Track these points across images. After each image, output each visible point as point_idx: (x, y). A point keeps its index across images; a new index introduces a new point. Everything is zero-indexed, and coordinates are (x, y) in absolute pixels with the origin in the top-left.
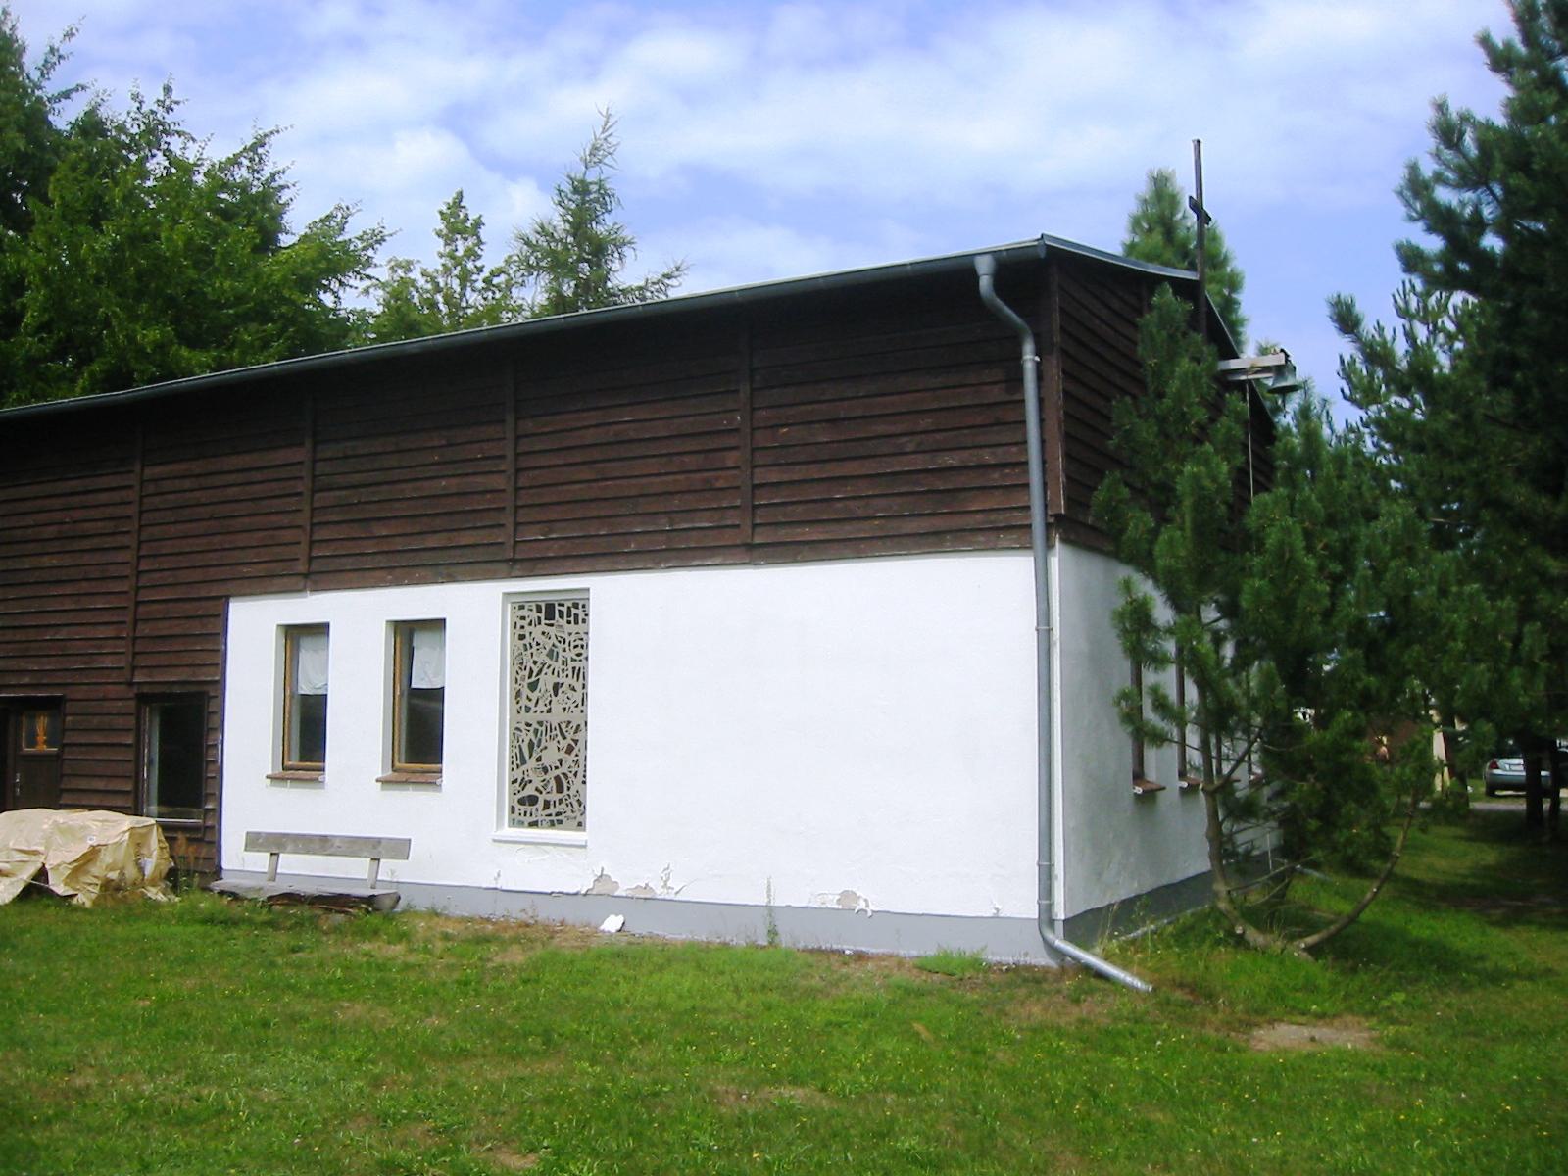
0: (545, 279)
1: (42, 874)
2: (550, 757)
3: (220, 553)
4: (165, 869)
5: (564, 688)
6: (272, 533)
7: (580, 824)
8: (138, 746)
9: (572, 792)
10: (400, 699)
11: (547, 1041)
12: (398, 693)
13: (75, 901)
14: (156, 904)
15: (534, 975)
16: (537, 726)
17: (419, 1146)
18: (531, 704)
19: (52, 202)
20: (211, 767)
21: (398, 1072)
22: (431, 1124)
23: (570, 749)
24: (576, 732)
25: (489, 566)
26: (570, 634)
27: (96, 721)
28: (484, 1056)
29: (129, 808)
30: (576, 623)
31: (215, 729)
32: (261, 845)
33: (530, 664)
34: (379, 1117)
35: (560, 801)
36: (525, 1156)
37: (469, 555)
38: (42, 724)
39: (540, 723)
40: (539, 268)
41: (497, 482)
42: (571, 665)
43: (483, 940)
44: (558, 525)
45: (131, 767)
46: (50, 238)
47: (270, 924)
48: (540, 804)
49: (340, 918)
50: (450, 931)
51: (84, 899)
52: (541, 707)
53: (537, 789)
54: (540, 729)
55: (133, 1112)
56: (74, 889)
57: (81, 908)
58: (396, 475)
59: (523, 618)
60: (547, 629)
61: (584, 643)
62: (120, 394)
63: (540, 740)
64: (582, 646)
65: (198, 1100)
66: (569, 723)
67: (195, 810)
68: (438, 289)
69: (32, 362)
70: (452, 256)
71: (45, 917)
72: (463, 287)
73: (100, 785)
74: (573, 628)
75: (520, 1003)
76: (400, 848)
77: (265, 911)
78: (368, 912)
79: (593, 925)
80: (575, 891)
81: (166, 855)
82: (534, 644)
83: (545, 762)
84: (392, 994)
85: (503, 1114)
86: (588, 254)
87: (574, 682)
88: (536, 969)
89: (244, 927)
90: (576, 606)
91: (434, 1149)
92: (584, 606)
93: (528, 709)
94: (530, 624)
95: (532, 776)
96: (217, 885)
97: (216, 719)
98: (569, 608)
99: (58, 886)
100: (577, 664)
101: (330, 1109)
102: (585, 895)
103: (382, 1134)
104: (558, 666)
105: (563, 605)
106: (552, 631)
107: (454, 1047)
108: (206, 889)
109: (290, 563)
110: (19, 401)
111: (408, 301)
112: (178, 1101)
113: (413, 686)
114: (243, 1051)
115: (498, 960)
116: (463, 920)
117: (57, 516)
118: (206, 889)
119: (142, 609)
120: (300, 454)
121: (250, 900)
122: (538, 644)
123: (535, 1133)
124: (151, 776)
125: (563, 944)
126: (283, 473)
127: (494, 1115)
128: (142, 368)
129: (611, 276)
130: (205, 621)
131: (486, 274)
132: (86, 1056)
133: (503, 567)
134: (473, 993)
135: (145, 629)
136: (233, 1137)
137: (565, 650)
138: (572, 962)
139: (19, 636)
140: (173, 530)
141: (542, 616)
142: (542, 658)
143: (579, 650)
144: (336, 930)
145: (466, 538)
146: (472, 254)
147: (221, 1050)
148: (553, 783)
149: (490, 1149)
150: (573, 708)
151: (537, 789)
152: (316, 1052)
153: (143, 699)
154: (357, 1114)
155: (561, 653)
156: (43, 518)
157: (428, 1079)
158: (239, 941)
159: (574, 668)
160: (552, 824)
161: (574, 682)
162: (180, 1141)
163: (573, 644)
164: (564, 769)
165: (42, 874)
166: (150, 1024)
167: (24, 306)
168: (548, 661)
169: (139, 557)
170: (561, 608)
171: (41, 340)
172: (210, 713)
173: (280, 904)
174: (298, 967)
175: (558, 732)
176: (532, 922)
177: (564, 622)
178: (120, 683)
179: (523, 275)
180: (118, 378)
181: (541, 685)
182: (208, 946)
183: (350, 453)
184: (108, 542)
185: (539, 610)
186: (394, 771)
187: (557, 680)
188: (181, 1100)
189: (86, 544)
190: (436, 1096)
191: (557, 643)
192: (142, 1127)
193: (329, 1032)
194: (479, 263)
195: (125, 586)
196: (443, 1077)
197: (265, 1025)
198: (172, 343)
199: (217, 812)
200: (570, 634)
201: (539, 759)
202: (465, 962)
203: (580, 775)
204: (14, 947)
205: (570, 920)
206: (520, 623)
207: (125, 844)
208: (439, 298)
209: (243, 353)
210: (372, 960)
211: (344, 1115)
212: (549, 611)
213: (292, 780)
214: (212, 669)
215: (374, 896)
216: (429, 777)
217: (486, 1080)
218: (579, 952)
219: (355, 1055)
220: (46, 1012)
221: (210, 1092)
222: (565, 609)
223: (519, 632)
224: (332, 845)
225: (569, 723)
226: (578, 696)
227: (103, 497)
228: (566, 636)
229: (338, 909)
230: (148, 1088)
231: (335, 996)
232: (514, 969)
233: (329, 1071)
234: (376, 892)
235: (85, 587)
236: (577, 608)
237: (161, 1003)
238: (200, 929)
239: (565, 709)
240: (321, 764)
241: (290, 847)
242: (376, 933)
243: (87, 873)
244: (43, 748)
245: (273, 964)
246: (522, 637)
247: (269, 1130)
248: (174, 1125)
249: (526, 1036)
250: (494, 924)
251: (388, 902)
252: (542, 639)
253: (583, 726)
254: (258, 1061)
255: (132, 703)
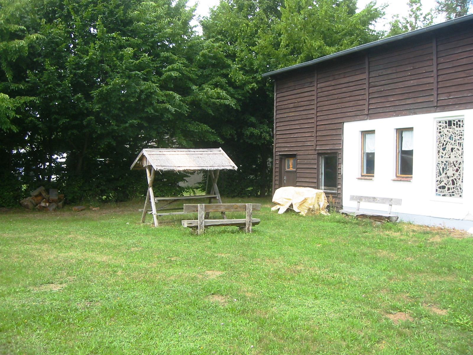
0: (445, 14)
1: (291, 205)
2: (450, 173)
3: (340, 109)
4: (327, 204)
5: (455, 149)
6: (356, 102)
7: (461, 196)
8: (318, 169)
9: (458, 185)
10: (398, 154)
11: (449, 270)
12: (398, 152)
13: (300, 214)
14: (324, 216)
15: (444, 246)
16: (446, 163)
17: (404, 302)
18: (443, 155)
19: (286, 7)
20: (339, 175)
21: (397, 275)
22: (408, 295)
23: (457, 170)
24: (459, 164)
25: (428, 109)
26: (457, 131)
27: (306, 161)
28: (427, 272)
29: (316, 187)
30: (460, 127)
31: (340, 163)
32: (354, 199)
33: (443, 142)
34: (391, 290)
35: (454, 188)
36: (442, 310)
37: (421, 106)
38: (291, 161)
39: (447, 162)
40: (442, 10)
41: (431, 80)
42: (458, 141)
43: (426, 233)
44: (453, 93)
45: (316, 175)
46: (287, 18)
47: (357, 224)
48: (446, 189)
49: (379, 223)
50: (415, 229)
51: (303, 213)
52: (447, 156)
53: (445, 184)
54: (446, 163)
55: (313, 279)
56: (300, 210)
57: (302, 216)
58: (396, 80)
59: (440, 126)
60: (449, 130)
61: (463, 134)
62: (310, 62)
63: (446, 167)
64: (462, 135)
65: (333, 278)
66: (457, 161)
67: (335, 188)
68: (407, 22)
69: (285, 56)
70: (412, 11)
71: (291, 218)
72: (416, 20)
73: (307, 180)
74: (458, 129)
75: (439, 255)
76: (399, 202)
77: (355, 219)
78: (388, 222)
79: (465, 230)
80: (458, 219)
81: (327, 201)
82: (444, 135)
83: (448, 175)
84: (396, 249)
85: (434, 294)
86: (460, 3)
87: (459, 147)
88: (445, 244)
89: (349, 224)
90: (459, 121)
91: (410, 304)
92: (462, 121)
93: (442, 157)
94: (443, 128)
95: (443, 179)
96: (341, 211)
97: (341, 160)
98: (457, 122)
99: (295, 209)
100: (460, 141)
101: (374, 285)
102: (462, 220)
103: (392, 295)
104: (453, 142)
105: (455, 121)
106: (451, 130)
107: (417, 268)
108: (338, 212)
109: (362, 111)
110: (281, 67)
111: (397, 27)
112: (327, 278)
113: (403, 149)
114: (348, 264)
115: (431, 240)
116: (419, 226)
117: (293, 101)
118: (338, 212)
119: (318, 127)
120: (365, 76)
121: (351, 216)
122: (446, 135)
123: (446, 302)
124: (322, 178)
125: (454, 236)
126: (360, 82)
127: (431, 294)
128: (315, 54)
129: (469, 10)
130: (337, 130)
131: (424, 15)
132: (301, 260)
133: (433, 109)
134: (423, 250)
135: (319, 134)
136: (344, 291)
137: (455, 136)
138: (458, 243)
139: (284, 136)
140: (326, 103)
141: (447, 125)
142: (447, 139)
143: (461, 136)
144: (377, 227)
145: (420, 100)
146: (418, 9)
147: (341, 262)
148: (451, 182)
149: (429, 306)
150: (458, 156)
151: (445, 184)
152: (371, 266)
153: (319, 154)
154: (384, 288)
155: (454, 138)
156: (289, 102)
157: (408, 279)
158: (348, 228)
159: (459, 143)
160: (451, 195)
161: (459, 147)
162: (327, 290)
163: (458, 134)
164: (455, 177)
165: (291, 205)
166: (320, 252)
167: (281, 40)
168: (449, 140)
169: (317, 112)
170: (454, 122)
171: (287, 49)
172: (339, 159)
173: (360, 218)
174: (366, 238)
175: (453, 165)
176: (443, 228)
177: (455, 127)
178: (313, 150)
179: (437, 14)
180: (309, 58)
181: (447, 148)
182: (338, 229)
183: (380, 74)
184: (308, 108)
185: (446, 123)
186: (396, 177)
187: (452, 147)
188: (328, 277)
189: (302, 109)
190: (410, 285)
191: (452, 134)
192: (316, 284)
193: (375, 260)
194: (421, 12)
195: (313, 121)
196: (413, 279)
197: (355, 255)
198: (324, 46)
199: (341, 189)
200: (457, 131)
201: (446, 174)
202: (420, 240)
203: (461, 179)
204: (283, 226)
205: (457, 228)
206: (439, 128)
207: (314, 198)
208: (408, 25)
209: (345, 46)
210: (389, 237)
211: (379, 288)
212: (450, 123)
213: (364, 179)
214: (339, 145)
215: (390, 217)
216: (408, 179)
217: (428, 281)
218: (460, 239)
219: (384, 268)
220: (291, 246)
221: (337, 275)
222: (455, 122)
223: (439, 131)
224: (377, 200)
225: (457, 161)
226: (460, 152)
227: (306, 94)
228: (456, 132)
229: (379, 220)
230: (318, 272)
231: (377, 248)
232: (437, 244)
233: (374, 272)
234: (391, 215)
235: (302, 121)
236: (460, 122)
237: (324, 246)
238: (336, 224)
239: (455, 157)
240: (373, 175)
241: (363, 200)
242: (390, 228)
243: (304, 206)
244: (291, 169)
245: (358, 236)
246: (440, 132)
247: (354, 290)
248: (326, 285)
249: (442, 267)
250: (430, 228)
251: (394, 219)
252: (447, 133)
253: (462, 163)
254: (352, 267)
255: (316, 156)
